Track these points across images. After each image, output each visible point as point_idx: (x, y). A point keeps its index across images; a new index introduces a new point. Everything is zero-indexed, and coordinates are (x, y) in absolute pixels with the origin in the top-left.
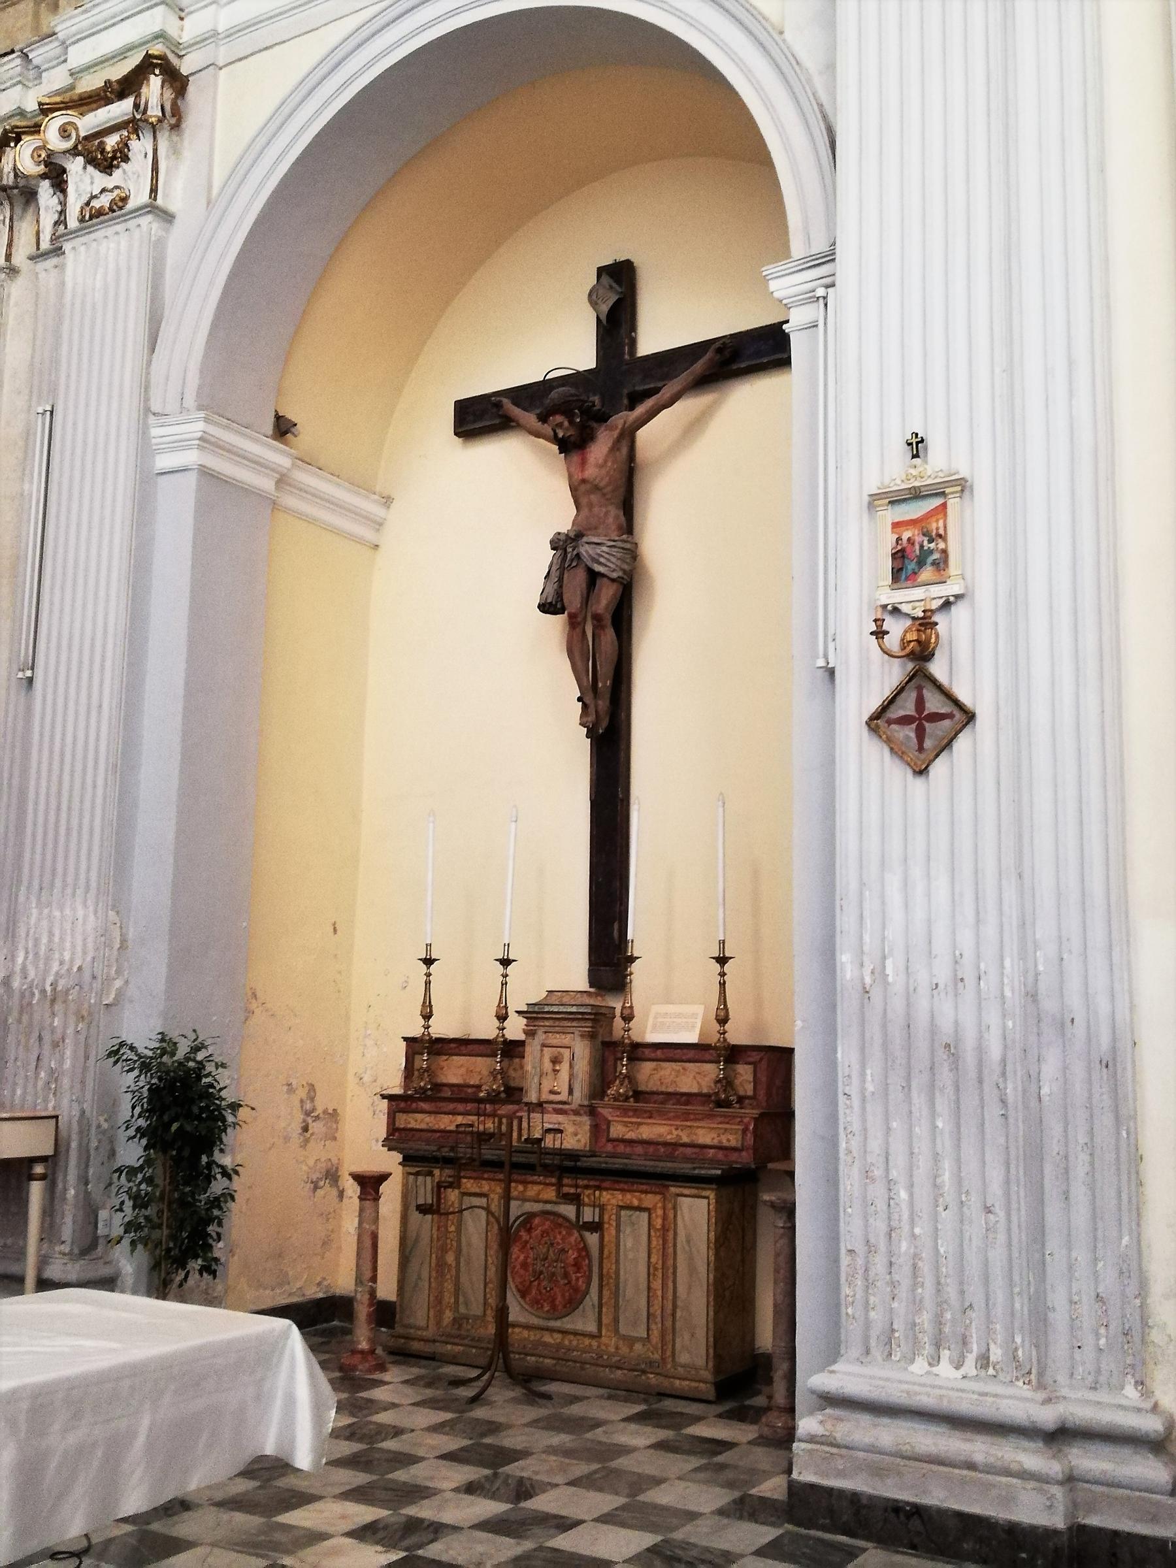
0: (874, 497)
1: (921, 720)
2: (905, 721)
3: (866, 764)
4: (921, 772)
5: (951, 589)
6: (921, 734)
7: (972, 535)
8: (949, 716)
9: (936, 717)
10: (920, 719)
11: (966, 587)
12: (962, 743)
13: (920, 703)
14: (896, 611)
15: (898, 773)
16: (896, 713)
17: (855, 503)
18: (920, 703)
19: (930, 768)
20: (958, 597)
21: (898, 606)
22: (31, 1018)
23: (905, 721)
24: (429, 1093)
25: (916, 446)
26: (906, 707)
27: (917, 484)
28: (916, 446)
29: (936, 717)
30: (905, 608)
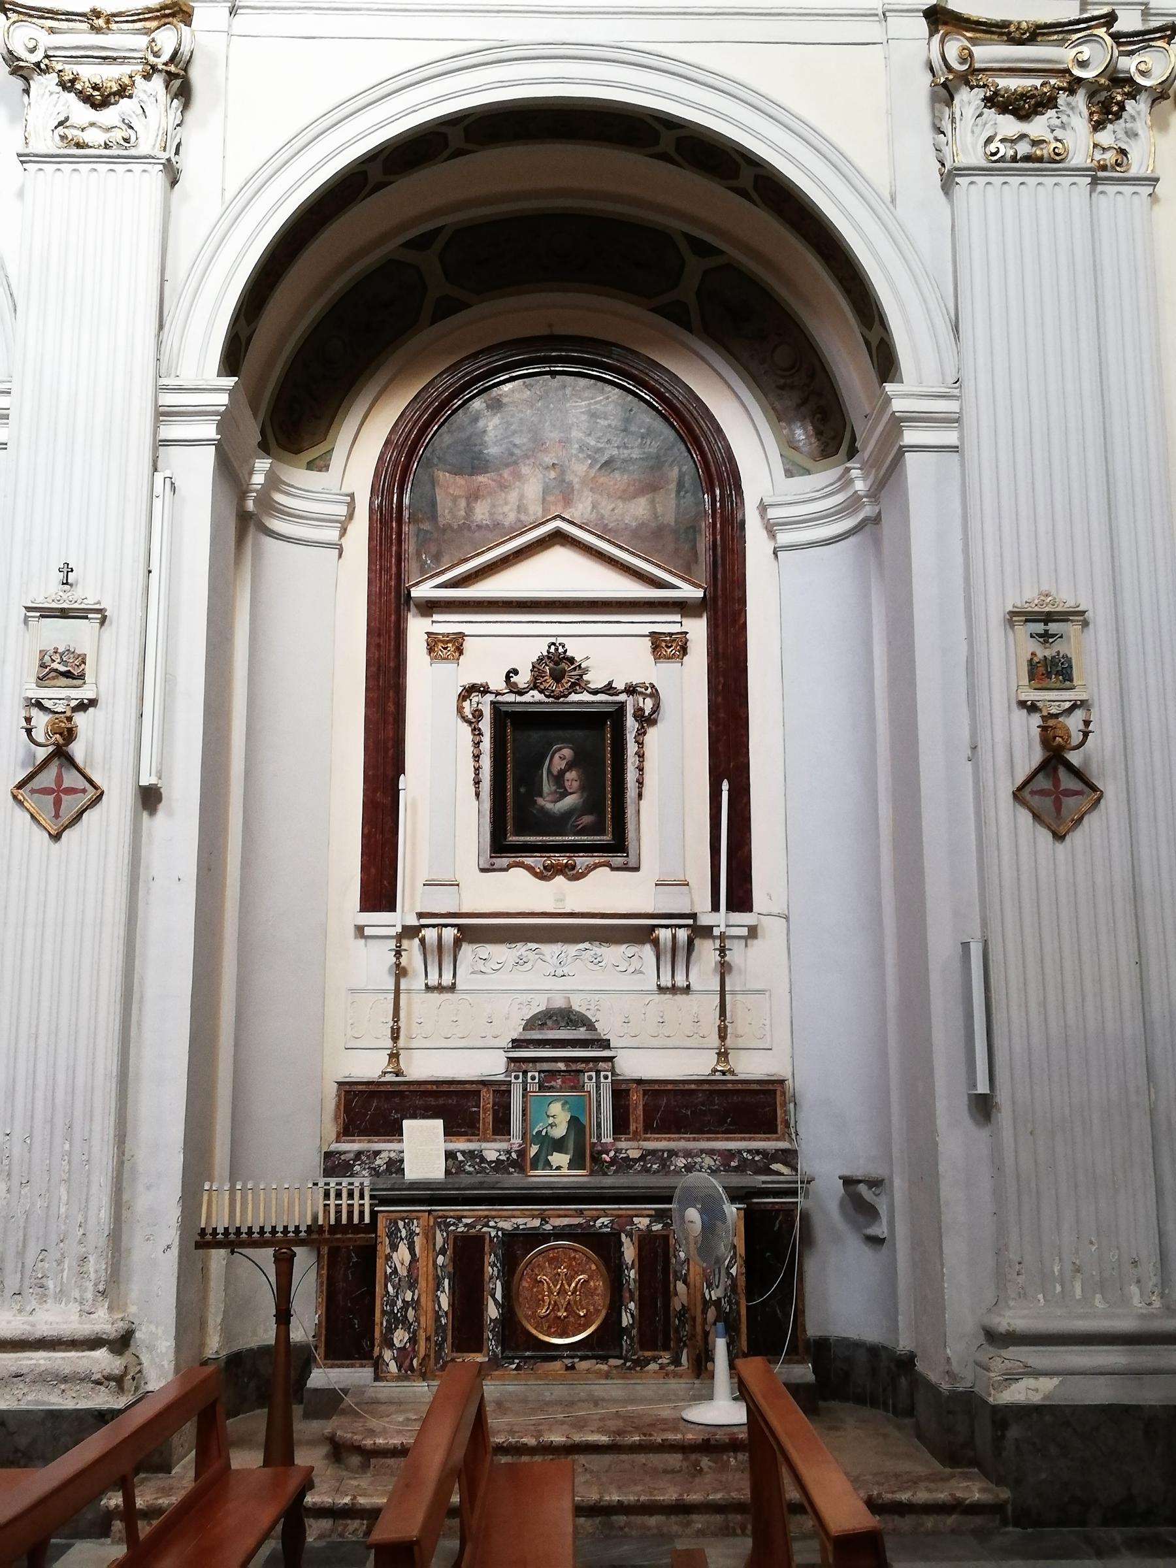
0: (1013, 614)
1: (1058, 795)
2: (46, 791)
3: (1017, 828)
4: (56, 837)
5: (86, 693)
6: (58, 803)
7: (1090, 652)
8: (84, 791)
9: (71, 791)
10: (59, 791)
11: (97, 694)
12: (1092, 822)
13: (59, 779)
14: (39, 705)
15: (1044, 836)
16: (36, 783)
17: (996, 617)
18: (59, 779)
19: (64, 834)
20: (93, 703)
21: (1038, 704)
22: (495, 1300)
23: (46, 791)
24: (327, 1235)
29: (71, 791)
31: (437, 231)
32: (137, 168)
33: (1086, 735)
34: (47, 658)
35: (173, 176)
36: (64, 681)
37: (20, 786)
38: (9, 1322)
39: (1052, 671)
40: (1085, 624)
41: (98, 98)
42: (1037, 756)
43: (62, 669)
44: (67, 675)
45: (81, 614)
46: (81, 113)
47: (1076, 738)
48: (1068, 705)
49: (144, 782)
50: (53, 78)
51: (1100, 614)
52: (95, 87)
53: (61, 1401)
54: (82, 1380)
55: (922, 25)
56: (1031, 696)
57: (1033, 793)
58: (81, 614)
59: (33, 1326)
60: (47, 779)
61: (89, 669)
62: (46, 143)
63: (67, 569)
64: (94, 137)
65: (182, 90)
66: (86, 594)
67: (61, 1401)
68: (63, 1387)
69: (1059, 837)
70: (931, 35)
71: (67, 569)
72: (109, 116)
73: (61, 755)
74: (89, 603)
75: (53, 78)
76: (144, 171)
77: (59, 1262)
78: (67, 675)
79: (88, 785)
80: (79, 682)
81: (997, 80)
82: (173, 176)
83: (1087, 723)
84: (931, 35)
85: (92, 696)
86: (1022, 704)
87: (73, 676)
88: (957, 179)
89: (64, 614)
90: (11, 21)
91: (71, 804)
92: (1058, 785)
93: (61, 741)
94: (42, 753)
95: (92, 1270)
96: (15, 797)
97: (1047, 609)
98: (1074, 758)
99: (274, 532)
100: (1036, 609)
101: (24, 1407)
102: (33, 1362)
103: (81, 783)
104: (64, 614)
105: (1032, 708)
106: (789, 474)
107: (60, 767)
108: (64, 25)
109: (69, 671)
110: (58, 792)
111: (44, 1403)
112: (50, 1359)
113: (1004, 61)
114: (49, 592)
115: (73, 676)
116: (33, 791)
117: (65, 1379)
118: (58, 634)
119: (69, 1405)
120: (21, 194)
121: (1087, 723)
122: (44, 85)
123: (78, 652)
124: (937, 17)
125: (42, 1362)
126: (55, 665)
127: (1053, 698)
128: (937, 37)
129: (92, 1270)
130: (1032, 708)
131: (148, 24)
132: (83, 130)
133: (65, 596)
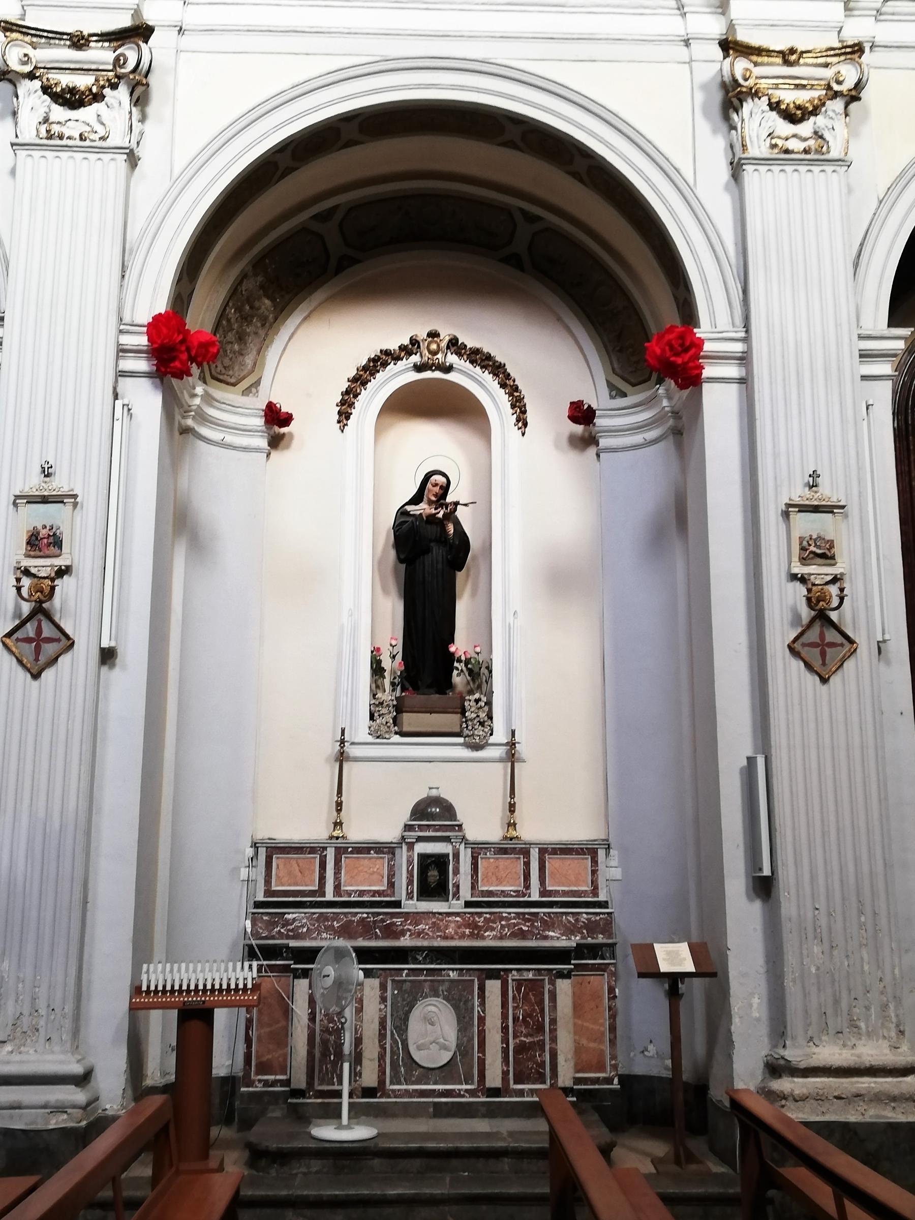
1: (823, 646)
2: (28, 640)
4: (36, 676)
8: (842, 645)
9: (832, 645)
13: (822, 636)
14: (27, 572)
15: (811, 680)
16: (805, 639)
18: (822, 636)
23: (28, 640)
25: (47, 473)
26: (813, 635)
27: (46, 493)
28: (47, 473)
30: (33, 571)
31: (336, 208)
32: (829, 169)
33: (842, 599)
34: (805, 543)
35: (133, 160)
36: (819, 561)
37: (9, 635)
38: (840, 1054)
39: (42, 542)
40: (846, 516)
41: (72, 99)
42: (806, 614)
43: (819, 551)
44: (823, 556)
45: (58, 500)
46: (784, 128)
47: (835, 602)
48: (829, 578)
49: (105, 644)
50: (37, 84)
51: (90, 499)
52: (799, 107)
53: (894, 1115)
54: (907, 1099)
55: (719, 53)
56: (798, 569)
57: (804, 645)
58: (58, 500)
59: (859, 1056)
60: (30, 630)
61: (836, 550)
62: (28, 133)
63: (815, 475)
64: (72, 130)
65: (140, 97)
66: (60, 484)
67: (894, 1115)
68: (893, 1104)
69: (824, 680)
70: (724, 58)
71: (815, 475)
72: (806, 128)
73: (41, 610)
74: (65, 490)
75: (765, 99)
76: (834, 171)
77: (868, 1008)
78: (823, 556)
79: (845, 641)
80: (832, 562)
81: (50, 76)
82: (133, 160)
83: (842, 590)
84: (724, 58)
85: (68, 563)
86: (794, 577)
87: (827, 557)
88: (744, 167)
89: (45, 500)
90: (9, 39)
91: (49, 649)
92: (823, 639)
93: (42, 598)
94: (26, 608)
95: (893, 1015)
96: (4, 644)
97: (816, 503)
98: (834, 616)
99: (205, 438)
100: (807, 503)
101: (868, 1120)
102: (866, 1085)
103: (839, 639)
104: (45, 500)
105: (803, 580)
106: (612, 397)
107: (822, 626)
108: (766, 59)
109: (824, 553)
110: (38, 640)
111: (887, 1118)
112: (875, 1082)
113: (52, 62)
114: (33, 483)
115: (827, 557)
116: (18, 640)
117: (894, 1099)
118: (807, 525)
119: (902, 1118)
120: (13, 172)
121: (842, 590)
122: (30, 90)
123: (827, 538)
124: (729, 46)
125: (873, 1085)
126: (812, 548)
127: (818, 571)
128: (728, 60)
129: (893, 1015)
130: (803, 580)
131: (829, 60)
132: (787, 140)
133: (46, 486)
